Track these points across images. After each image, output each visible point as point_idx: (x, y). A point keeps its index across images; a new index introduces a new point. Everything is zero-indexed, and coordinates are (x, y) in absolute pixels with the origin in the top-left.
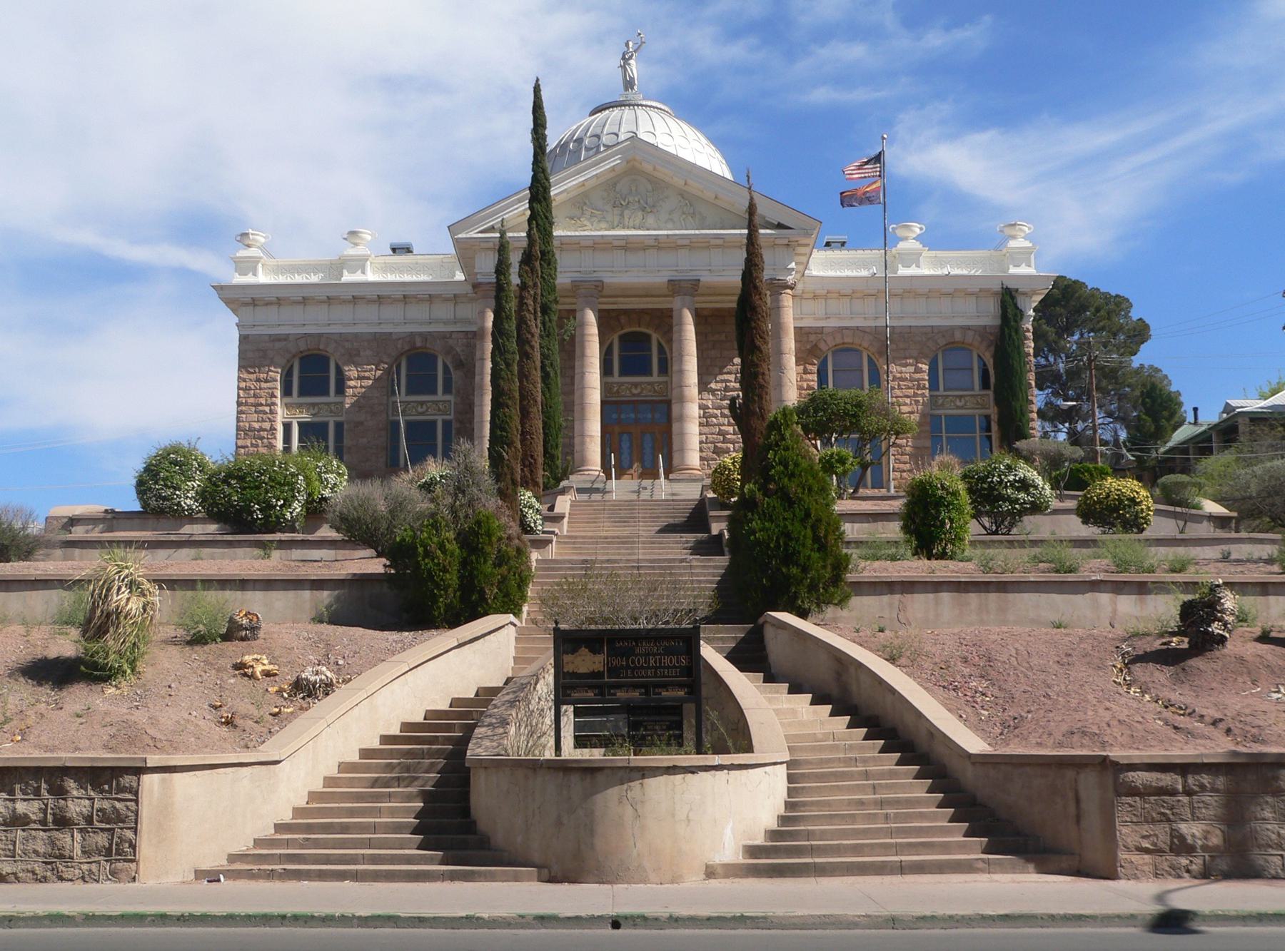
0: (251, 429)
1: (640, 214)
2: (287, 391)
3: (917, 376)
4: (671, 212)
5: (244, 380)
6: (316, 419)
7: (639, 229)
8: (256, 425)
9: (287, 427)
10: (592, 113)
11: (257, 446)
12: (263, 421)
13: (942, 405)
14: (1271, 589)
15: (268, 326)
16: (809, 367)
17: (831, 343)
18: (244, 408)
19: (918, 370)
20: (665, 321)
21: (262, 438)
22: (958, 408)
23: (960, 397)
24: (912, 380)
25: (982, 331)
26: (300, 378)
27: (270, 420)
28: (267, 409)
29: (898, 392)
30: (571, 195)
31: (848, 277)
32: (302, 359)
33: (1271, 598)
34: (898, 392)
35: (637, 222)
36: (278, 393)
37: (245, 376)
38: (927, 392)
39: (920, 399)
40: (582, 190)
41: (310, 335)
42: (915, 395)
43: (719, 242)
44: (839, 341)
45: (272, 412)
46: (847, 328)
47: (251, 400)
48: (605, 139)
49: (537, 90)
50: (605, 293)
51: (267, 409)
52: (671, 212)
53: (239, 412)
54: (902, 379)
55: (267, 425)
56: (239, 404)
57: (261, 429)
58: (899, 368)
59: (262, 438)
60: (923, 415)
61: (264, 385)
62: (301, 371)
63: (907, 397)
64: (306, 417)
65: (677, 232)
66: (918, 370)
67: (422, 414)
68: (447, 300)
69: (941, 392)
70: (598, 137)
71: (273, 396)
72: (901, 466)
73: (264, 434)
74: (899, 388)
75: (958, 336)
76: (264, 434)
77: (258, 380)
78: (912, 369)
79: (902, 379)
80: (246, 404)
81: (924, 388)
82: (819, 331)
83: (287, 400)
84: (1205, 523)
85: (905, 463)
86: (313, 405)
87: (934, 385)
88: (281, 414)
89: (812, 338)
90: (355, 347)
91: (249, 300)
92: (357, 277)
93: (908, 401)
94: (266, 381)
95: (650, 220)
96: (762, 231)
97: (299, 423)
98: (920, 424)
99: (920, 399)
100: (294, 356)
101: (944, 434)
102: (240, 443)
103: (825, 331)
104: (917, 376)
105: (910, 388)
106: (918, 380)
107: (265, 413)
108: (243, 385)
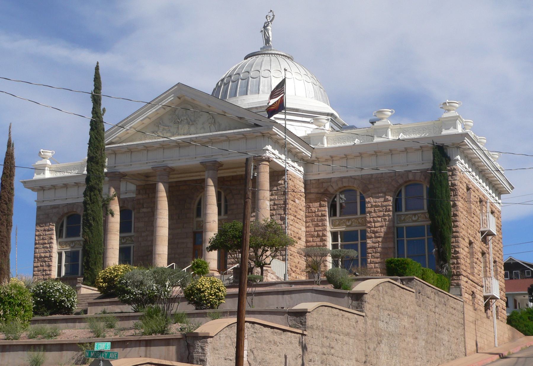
0: (41, 257)
1: (187, 126)
2: (59, 235)
3: (385, 203)
4: (203, 124)
5: (38, 231)
6: (74, 249)
7: (186, 135)
8: (43, 255)
9: (60, 254)
10: (246, 58)
11: (43, 266)
12: (46, 252)
13: (404, 220)
14: (48, 347)
15: (50, 201)
16: (322, 203)
17: (336, 187)
18: (37, 246)
19: (386, 200)
20: (201, 186)
21: (45, 262)
22: (414, 221)
23: (415, 215)
24: (382, 206)
25: (424, 172)
26: (67, 227)
27: (50, 252)
28: (48, 246)
29: (374, 215)
30: (153, 119)
31: (339, 147)
32: (68, 218)
33: (64, 352)
34: (374, 215)
35: (185, 131)
36: (54, 237)
37: (39, 228)
38: (391, 213)
39: (387, 218)
40: (158, 116)
41: (70, 204)
42: (384, 215)
43: (224, 138)
44: (340, 185)
45: (50, 247)
46: (345, 177)
47: (41, 242)
48: (252, 74)
49: (97, 68)
50: (224, 167)
51: (48, 246)
52: (203, 124)
53: (36, 248)
54: (376, 206)
55: (48, 255)
56: (36, 244)
57: (45, 257)
58: (375, 200)
59: (45, 262)
60: (389, 228)
61: (47, 233)
62: (68, 223)
63: (379, 217)
64: (68, 249)
65: (201, 135)
66: (386, 200)
67: (416, 221)
68: (386, 154)
69: (404, 212)
70: (239, 74)
71: (51, 238)
72: (375, 260)
73: (46, 259)
74: (375, 212)
75: (411, 177)
76: (46, 259)
77: (45, 230)
78: (382, 199)
79: (376, 206)
80: (39, 244)
81: (389, 211)
82: (329, 180)
83: (60, 240)
84: (346, 298)
85: (377, 258)
86: (72, 242)
87: (397, 207)
88: (55, 247)
89: (325, 185)
90: (370, 184)
91: (403, 149)
92: (451, 131)
93: (379, 219)
94: (48, 231)
95: (192, 129)
96: (106, 147)
97: (65, 252)
98: (386, 233)
99: (387, 218)
100: (63, 216)
101: (405, 239)
102: (36, 265)
103: (333, 180)
104: (385, 203)
105: (381, 211)
106: (386, 206)
107: (47, 248)
108: (38, 233)
